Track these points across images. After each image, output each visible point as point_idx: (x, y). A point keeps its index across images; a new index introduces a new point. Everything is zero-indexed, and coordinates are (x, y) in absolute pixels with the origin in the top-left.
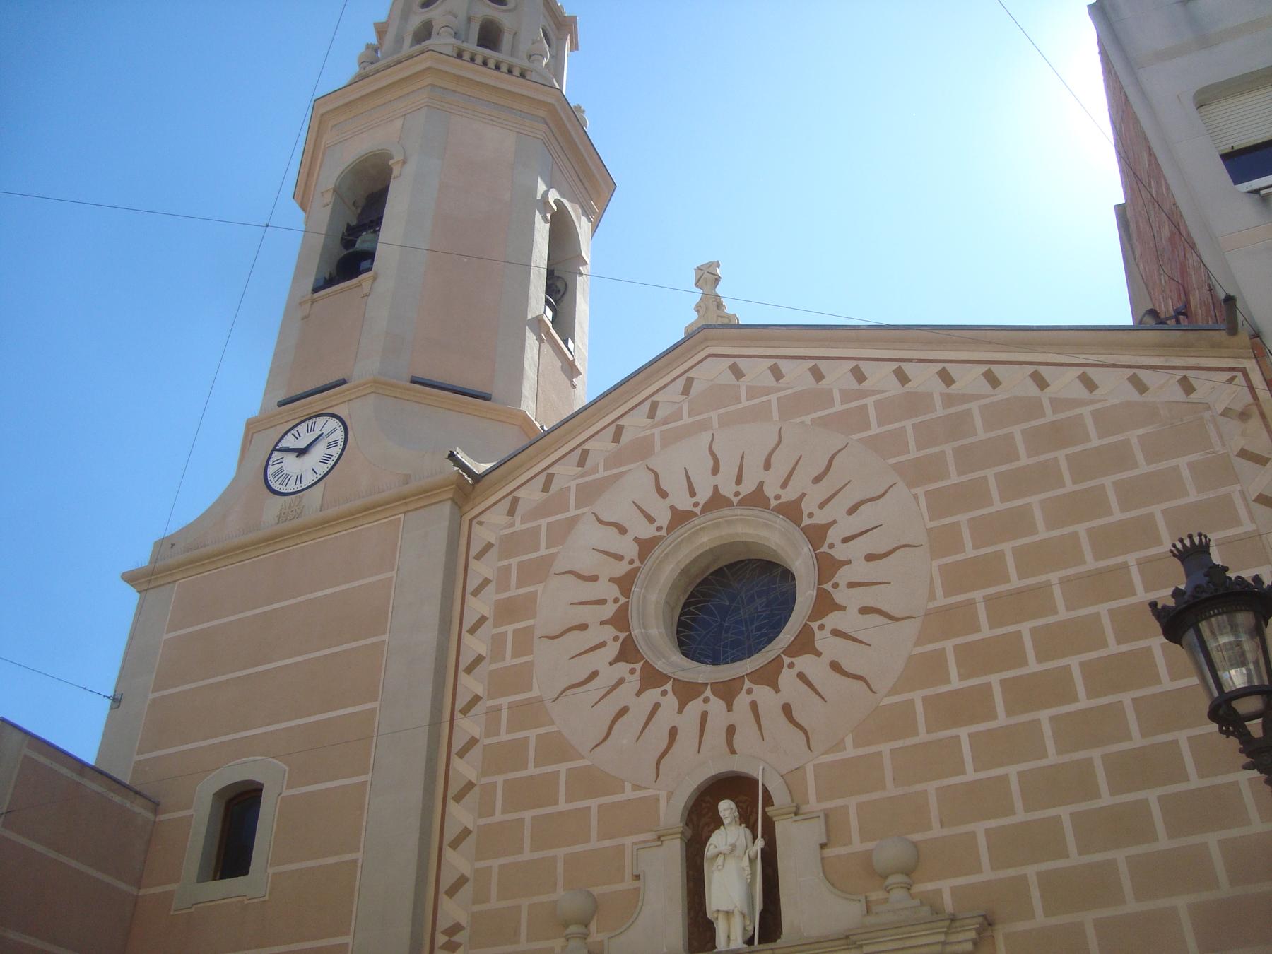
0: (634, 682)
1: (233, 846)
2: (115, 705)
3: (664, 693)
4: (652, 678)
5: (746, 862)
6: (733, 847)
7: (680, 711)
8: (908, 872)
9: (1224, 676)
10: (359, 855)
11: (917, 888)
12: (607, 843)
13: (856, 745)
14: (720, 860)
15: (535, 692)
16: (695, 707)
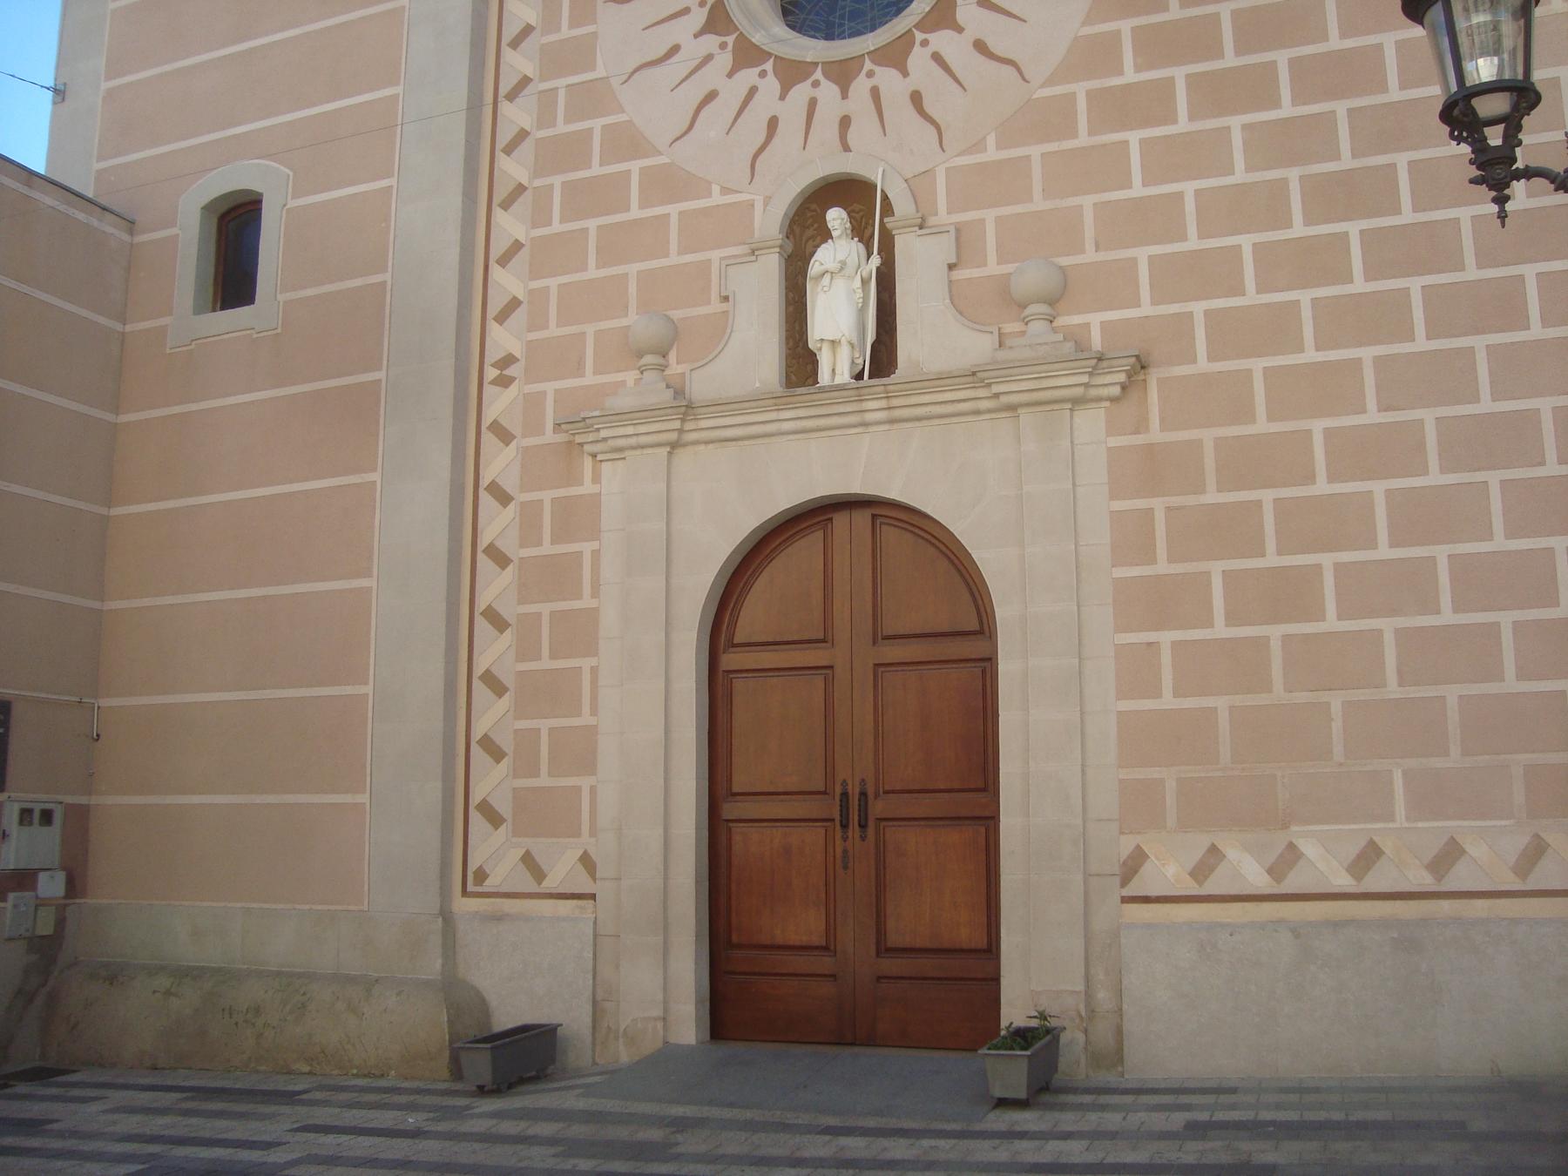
0: (725, 60)
1: (233, 269)
2: (59, 99)
3: (763, 74)
4: (748, 54)
5: (857, 283)
6: (843, 265)
7: (782, 97)
8: (1052, 302)
9: (1468, 67)
10: (387, 277)
11: (1061, 321)
12: (688, 258)
13: (999, 147)
14: (826, 280)
15: (600, 72)
16: (801, 92)
